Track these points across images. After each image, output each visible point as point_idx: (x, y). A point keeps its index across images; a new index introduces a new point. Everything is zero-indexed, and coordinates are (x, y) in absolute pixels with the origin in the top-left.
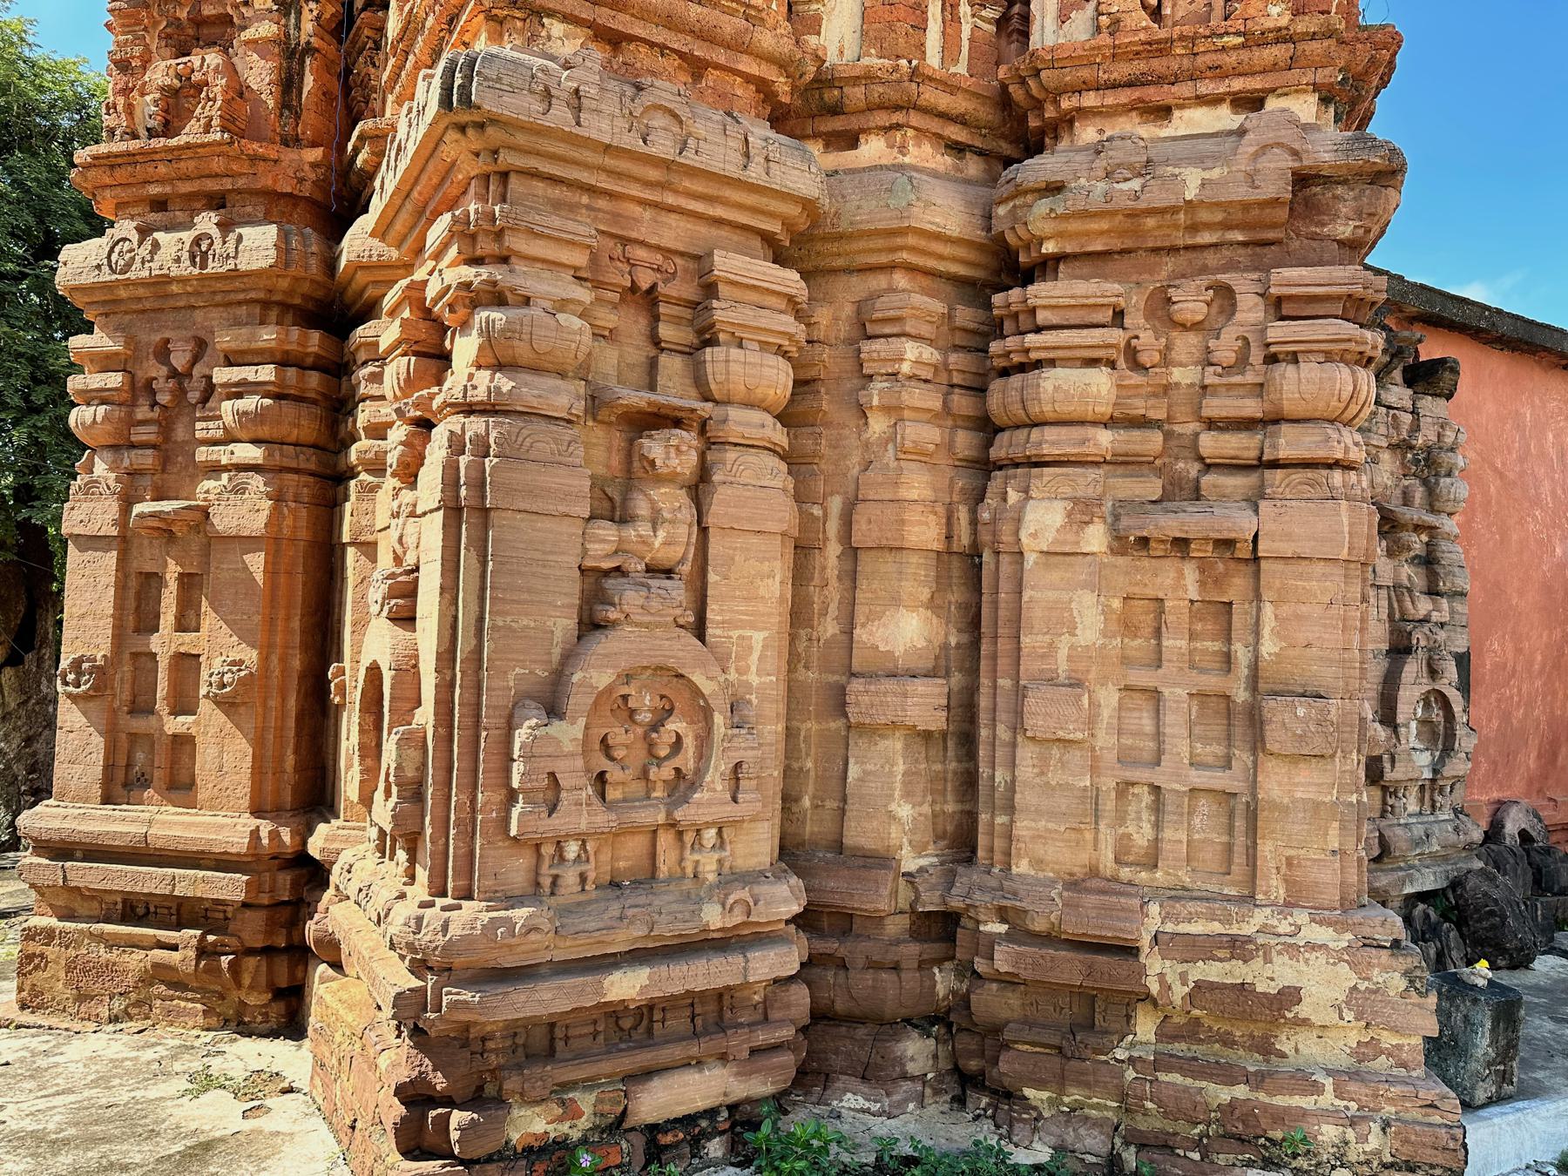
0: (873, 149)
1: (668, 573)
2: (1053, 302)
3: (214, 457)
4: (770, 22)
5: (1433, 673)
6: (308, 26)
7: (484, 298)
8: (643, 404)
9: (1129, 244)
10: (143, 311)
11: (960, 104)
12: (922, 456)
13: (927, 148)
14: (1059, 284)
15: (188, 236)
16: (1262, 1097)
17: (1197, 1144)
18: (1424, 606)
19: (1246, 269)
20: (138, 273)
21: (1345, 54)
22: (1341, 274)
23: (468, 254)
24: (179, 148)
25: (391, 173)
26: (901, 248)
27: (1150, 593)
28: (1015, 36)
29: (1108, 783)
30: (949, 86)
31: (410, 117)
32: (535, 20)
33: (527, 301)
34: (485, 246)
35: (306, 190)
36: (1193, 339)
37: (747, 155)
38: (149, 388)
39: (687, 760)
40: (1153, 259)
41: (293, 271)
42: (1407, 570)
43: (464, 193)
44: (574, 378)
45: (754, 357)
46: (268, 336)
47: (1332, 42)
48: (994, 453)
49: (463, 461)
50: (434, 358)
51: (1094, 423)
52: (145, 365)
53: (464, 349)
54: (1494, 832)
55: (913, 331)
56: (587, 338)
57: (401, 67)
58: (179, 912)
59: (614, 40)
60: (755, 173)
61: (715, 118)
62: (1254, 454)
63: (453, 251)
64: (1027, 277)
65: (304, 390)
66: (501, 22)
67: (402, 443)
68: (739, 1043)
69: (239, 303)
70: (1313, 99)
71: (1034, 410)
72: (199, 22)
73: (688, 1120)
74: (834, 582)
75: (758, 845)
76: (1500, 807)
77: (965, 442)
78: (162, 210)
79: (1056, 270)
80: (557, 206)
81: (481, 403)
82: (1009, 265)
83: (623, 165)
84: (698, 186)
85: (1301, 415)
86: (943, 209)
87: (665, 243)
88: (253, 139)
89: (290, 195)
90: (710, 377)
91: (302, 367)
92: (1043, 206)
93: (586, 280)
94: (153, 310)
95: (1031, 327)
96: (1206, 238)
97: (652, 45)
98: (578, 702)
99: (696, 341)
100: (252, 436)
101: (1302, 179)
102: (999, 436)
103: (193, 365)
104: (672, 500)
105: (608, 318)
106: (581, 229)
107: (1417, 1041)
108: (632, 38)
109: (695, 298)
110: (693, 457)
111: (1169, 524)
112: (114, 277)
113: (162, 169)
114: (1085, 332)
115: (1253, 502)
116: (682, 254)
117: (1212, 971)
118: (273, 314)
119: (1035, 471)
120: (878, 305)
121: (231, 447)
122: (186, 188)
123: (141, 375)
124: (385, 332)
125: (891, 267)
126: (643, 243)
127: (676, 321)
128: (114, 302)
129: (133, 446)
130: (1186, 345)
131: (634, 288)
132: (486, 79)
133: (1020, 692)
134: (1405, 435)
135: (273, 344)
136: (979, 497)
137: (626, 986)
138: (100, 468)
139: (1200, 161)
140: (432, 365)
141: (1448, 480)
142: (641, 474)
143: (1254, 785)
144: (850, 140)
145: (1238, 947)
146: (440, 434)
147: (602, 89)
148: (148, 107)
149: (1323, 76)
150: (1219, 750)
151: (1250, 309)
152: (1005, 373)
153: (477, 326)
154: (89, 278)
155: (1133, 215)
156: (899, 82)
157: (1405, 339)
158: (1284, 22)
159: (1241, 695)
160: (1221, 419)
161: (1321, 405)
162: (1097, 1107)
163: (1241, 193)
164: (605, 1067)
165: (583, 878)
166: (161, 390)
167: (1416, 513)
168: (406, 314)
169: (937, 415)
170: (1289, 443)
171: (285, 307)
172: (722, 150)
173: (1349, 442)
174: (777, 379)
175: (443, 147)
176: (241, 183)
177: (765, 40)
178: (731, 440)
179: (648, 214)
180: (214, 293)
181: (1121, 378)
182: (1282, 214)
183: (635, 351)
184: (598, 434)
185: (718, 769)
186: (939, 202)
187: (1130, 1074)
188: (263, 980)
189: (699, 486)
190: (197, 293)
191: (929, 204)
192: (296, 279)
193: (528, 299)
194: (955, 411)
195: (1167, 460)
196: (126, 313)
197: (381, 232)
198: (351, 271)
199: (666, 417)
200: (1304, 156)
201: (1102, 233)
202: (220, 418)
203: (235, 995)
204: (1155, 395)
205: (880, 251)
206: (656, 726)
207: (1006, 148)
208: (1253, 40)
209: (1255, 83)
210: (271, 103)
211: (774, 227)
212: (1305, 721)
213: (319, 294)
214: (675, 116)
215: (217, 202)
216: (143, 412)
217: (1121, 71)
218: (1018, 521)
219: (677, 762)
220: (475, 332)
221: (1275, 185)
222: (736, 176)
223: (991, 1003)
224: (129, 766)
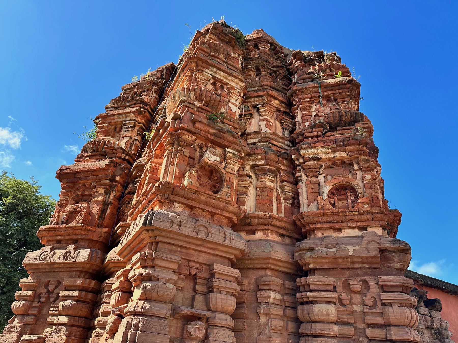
0: (259, 235)
2: (315, 283)
3: (53, 320)
4: (232, 204)
6: (112, 198)
7: (145, 278)
8: (189, 313)
9: (335, 266)
10: (45, 272)
11: (283, 224)
12: (277, 331)
13: (274, 235)
14: (316, 277)
15: (64, 251)
19: (370, 276)
20: (47, 261)
21: (387, 218)
22: (399, 279)
23: (143, 264)
24: (69, 227)
25: (126, 239)
26: (269, 263)
28: (296, 207)
30: (279, 220)
31: (135, 225)
32: (172, 203)
33: (158, 280)
34: (149, 263)
35: (101, 239)
36: (358, 296)
37: (225, 237)
38: (39, 297)
40: (342, 271)
41: (91, 262)
43: (145, 246)
44: (169, 303)
45: (224, 297)
46: (79, 282)
47: (383, 214)
49: (130, 332)
50: (127, 293)
51: (332, 323)
52: (40, 288)
53: (137, 293)
55: (273, 288)
56: (174, 291)
57: (134, 211)
59: (191, 208)
60: (227, 242)
61: (217, 228)
62: (384, 337)
63: (139, 264)
64: (306, 273)
65: (86, 299)
66: (163, 203)
67: (112, 323)
69: (74, 271)
70: (380, 229)
71: (312, 317)
72: (83, 195)
77: (291, 326)
78: (60, 243)
79: (314, 272)
80: (171, 251)
81: (139, 312)
82: (299, 271)
83: (191, 240)
84: (211, 246)
85: (397, 324)
86: (280, 253)
87: (200, 261)
88: (89, 226)
89: (96, 240)
90: (211, 303)
91: (87, 291)
92: (308, 254)
93: (176, 272)
94: (48, 272)
95: (309, 290)
96: (357, 266)
97: (201, 209)
99: (207, 291)
100: (66, 313)
101: (382, 251)
102: (302, 325)
103: (55, 289)
105: (181, 284)
106: (177, 258)
108: (196, 207)
109: (208, 277)
110: (204, 331)
112: (41, 262)
113: (63, 232)
114: (325, 293)
116: (205, 264)
119: (315, 339)
120: (262, 280)
121: (58, 317)
122: (68, 237)
123: (38, 292)
124: (114, 283)
125: (266, 269)
126: (194, 261)
127: (202, 284)
128: (37, 269)
129: (28, 315)
130: (356, 298)
131: (190, 274)
132: (156, 218)
134: (429, 324)
135: (80, 284)
138: (16, 322)
139: (352, 244)
140: (126, 295)
141: (448, 340)
142: (186, 337)
144: (253, 233)
146: (124, 322)
147: (187, 221)
148: (64, 216)
149: (381, 223)
152: (302, 303)
153: (142, 287)
154: (31, 262)
155: (335, 258)
156: (266, 218)
157: (422, 293)
158: (369, 209)
160: (372, 324)
161: (402, 321)
163: (365, 254)
166: (43, 297)
168: (122, 279)
169: (282, 317)
171: (87, 272)
172: (218, 236)
173: (414, 334)
174: (231, 303)
175: (142, 235)
176: (83, 237)
177: (231, 208)
178: (216, 325)
179: (196, 253)
180: (67, 268)
181: (338, 308)
182: (379, 260)
183: (188, 294)
184: (174, 322)
186: (279, 251)
190: (62, 268)
191: (276, 251)
192: (92, 265)
193: (158, 279)
194: (287, 315)
195: (356, 337)
196: (40, 272)
197: (120, 254)
198: (108, 263)
199: (196, 317)
200: (381, 244)
201: (326, 263)
202: (58, 307)
204: (349, 314)
205: (262, 264)
207: (296, 236)
208: (362, 213)
209: (364, 224)
210: (97, 216)
211: (232, 257)
213: (98, 269)
214: (206, 227)
215: (75, 242)
217: (326, 219)
220: (141, 289)
221: (374, 251)
222: (221, 243)
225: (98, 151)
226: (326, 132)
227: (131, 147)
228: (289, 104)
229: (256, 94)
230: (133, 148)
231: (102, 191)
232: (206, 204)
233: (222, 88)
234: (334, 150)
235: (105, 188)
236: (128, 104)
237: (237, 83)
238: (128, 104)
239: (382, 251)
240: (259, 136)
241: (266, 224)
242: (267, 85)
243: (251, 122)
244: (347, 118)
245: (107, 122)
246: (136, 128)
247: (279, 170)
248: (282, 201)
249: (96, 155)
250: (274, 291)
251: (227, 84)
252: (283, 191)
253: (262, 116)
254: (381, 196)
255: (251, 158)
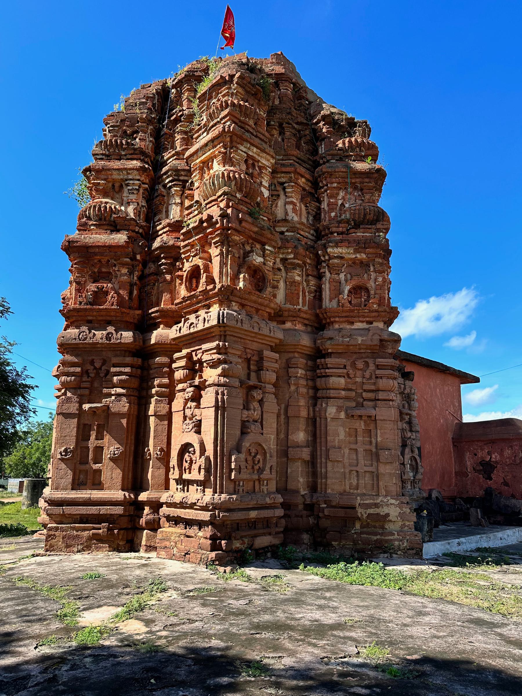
0: (288, 325)
1: (256, 421)
5: (412, 451)
6: (135, 278)
11: (307, 316)
16: (383, 537)
17: (370, 550)
18: (409, 434)
24: (103, 309)
27: (354, 427)
29: (347, 471)
30: (306, 313)
33: (231, 363)
36: (360, 372)
39: (261, 465)
42: (405, 425)
45: (271, 373)
48: (318, 395)
54: (430, 497)
58: (98, 519)
60: (272, 334)
68: (273, 530)
70: (382, 323)
71: (328, 386)
73: (263, 548)
74: (283, 425)
75: (273, 486)
76: (431, 491)
77: (311, 392)
83: (248, 333)
86: (306, 341)
91: (137, 368)
96: (362, 351)
98: (244, 450)
101: (381, 340)
104: (256, 404)
107: (412, 523)
111: (358, 412)
115: (375, 408)
117: (371, 511)
118: (127, 354)
125: (294, 352)
130: (359, 373)
133: (328, 451)
136: (315, 405)
137: (253, 514)
139: (361, 335)
143: (378, 470)
144: (284, 323)
145: (376, 505)
150: (370, 462)
151: (372, 367)
159: (374, 450)
162: (348, 545)
163: (369, 343)
164: (249, 533)
165: (243, 490)
167: (406, 411)
170: (381, 395)
171: (130, 352)
176: (118, 319)
179: (250, 342)
182: (378, 348)
185: (268, 466)
187: (355, 536)
188: (125, 537)
189: (261, 402)
190: (105, 347)
203: (116, 542)
206: (255, 456)
208: (371, 311)
209: (371, 319)
210: (127, 298)
212: (387, 455)
216: (85, 379)
217: (344, 314)
218: (326, 411)
219: (259, 465)
221: (376, 342)
223: (325, 523)
224: (79, 479)
225: (105, 220)
226: (350, 228)
227: (139, 215)
228: (315, 184)
229: (284, 169)
230: (142, 217)
231: (125, 271)
232: (255, 302)
233: (253, 166)
234: (356, 251)
235: (128, 268)
236: (123, 153)
237: (268, 160)
238: (123, 153)
239: (381, 340)
240: (288, 224)
241: (295, 316)
242: (293, 155)
243: (277, 204)
244: (370, 217)
245: (103, 177)
246: (141, 191)
247: (305, 263)
248: (307, 294)
249: (104, 225)
250: (300, 368)
251: (259, 161)
252: (308, 285)
253: (289, 197)
254: (387, 296)
255: (282, 251)
